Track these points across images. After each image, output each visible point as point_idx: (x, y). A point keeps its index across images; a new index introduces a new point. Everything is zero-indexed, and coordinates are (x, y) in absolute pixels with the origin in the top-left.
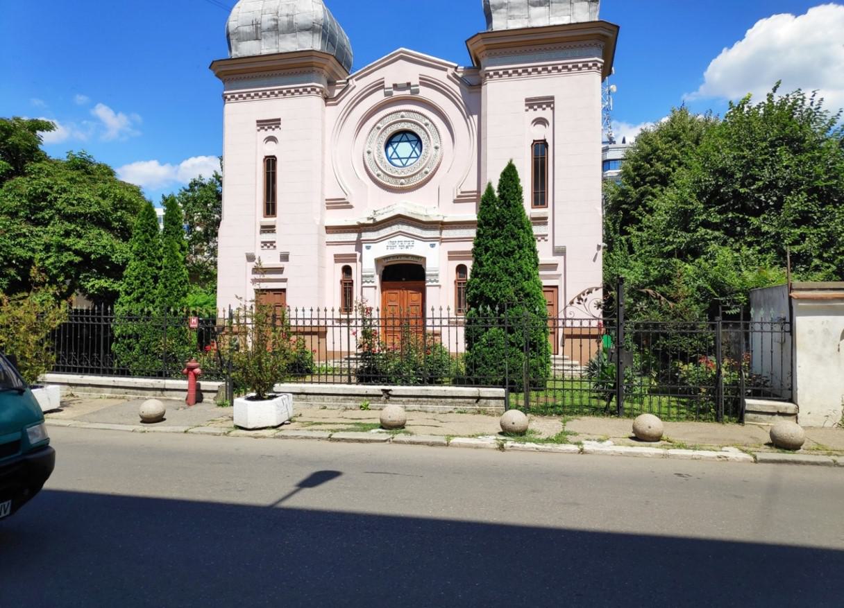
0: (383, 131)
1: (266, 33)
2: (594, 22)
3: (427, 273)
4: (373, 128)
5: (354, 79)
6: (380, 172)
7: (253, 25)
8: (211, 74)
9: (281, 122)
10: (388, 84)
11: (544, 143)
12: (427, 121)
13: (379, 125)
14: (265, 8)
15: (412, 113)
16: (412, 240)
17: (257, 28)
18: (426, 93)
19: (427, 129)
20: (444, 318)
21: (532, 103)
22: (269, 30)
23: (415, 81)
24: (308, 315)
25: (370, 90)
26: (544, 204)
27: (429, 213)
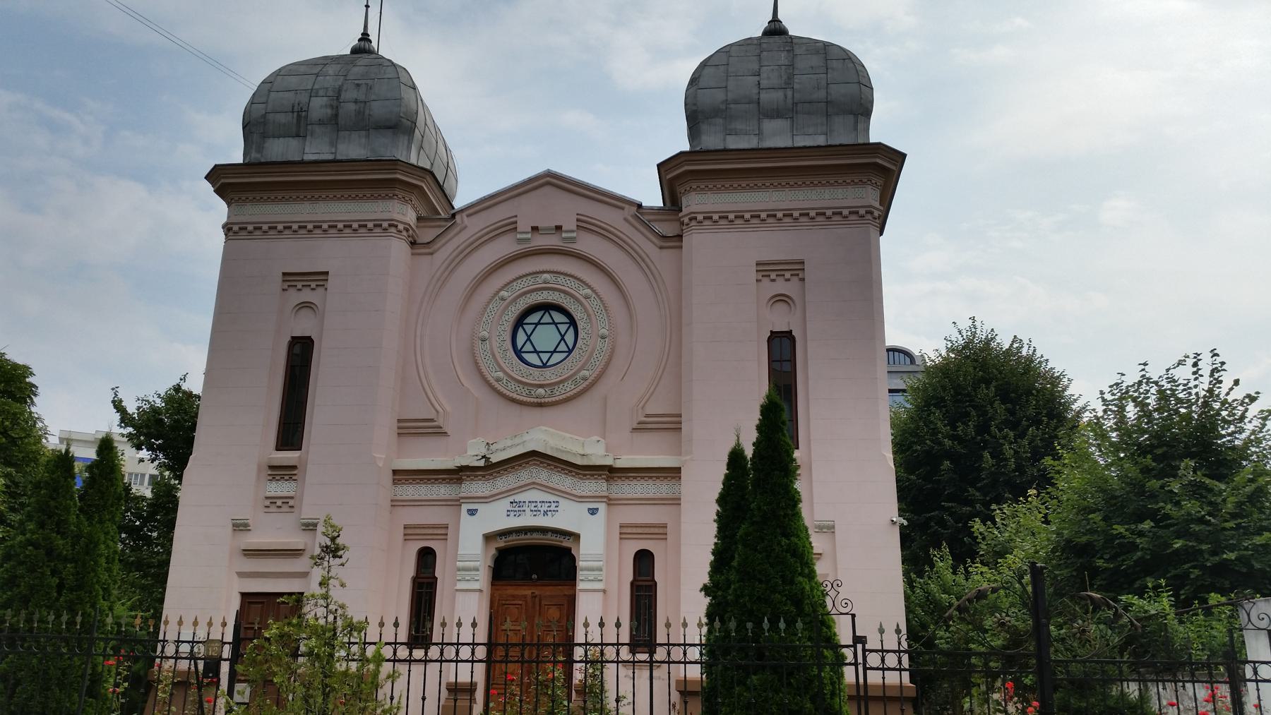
0: (511, 303)
1: (317, 129)
2: (819, 147)
3: (581, 564)
4: (493, 297)
5: (464, 214)
6: (500, 374)
7: (293, 112)
8: (208, 187)
9: (329, 277)
10: (524, 225)
11: (788, 335)
12: (588, 291)
13: (503, 293)
14: (316, 87)
15: (562, 277)
16: (556, 499)
17: (299, 117)
18: (589, 244)
19: (586, 304)
20: (467, 661)
21: (766, 269)
22: (321, 123)
23: (569, 224)
25: (488, 229)
26: (281, 446)
27: (588, 451)
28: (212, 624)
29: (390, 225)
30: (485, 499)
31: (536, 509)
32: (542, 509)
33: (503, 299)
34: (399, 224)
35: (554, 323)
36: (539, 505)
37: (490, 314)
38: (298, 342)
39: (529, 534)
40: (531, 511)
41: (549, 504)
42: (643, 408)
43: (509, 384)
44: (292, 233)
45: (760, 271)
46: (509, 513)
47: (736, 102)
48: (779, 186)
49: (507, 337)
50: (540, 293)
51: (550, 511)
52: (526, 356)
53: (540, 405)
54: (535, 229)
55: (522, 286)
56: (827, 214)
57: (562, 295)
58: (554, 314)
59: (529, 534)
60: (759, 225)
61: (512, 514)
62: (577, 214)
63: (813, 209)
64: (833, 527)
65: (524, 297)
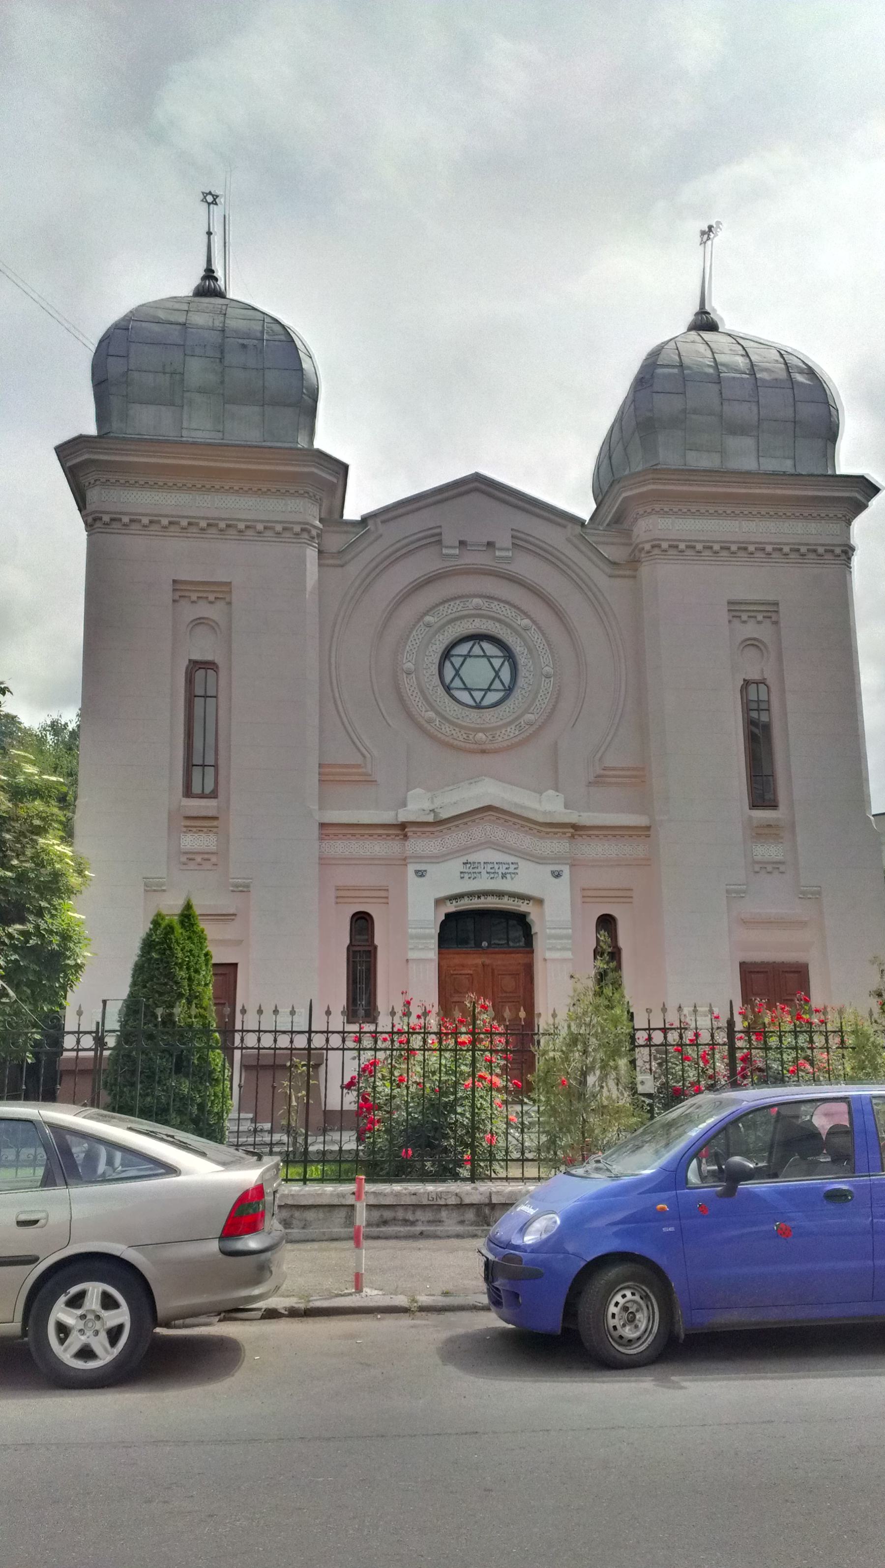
2: (785, 474)
5: (379, 520)
6: (431, 714)
10: (450, 538)
12: (526, 622)
13: (428, 619)
16: (512, 859)
22: (201, 391)
24: (284, 1023)
28: (395, 1013)
29: (303, 530)
30: (437, 859)
31: (492, 871)
32: (500, 872)
33: (429, 625)
34: (122, 517)
35: (466, 657)
36: (496, 866)
37: (414, 643)
38: (200, 668)
39: (482, 898)
40: (487, 873)
41: (507, 866)
42: (600, 759)
43: (443, 727)
44: (141, 528)
45: (731, 610)
46: (462, 876)
47: (695, 411)
48: (750, 515)
49: (435, 669)
50: (484, 620)
51: (510, 873)
52: (457, 694)
53: (483, 752)
54: (462, 543)
55: (450, 611)
56: (295, 530)
57: (497, 624)
58: (486, 645)
59: (482, 898)
60: (728, 559)
61: (466, 876)
62: (512, 530)
63: (787, 544)
64: (819, 893)
65: (453, 624)
